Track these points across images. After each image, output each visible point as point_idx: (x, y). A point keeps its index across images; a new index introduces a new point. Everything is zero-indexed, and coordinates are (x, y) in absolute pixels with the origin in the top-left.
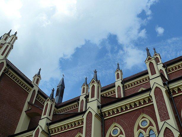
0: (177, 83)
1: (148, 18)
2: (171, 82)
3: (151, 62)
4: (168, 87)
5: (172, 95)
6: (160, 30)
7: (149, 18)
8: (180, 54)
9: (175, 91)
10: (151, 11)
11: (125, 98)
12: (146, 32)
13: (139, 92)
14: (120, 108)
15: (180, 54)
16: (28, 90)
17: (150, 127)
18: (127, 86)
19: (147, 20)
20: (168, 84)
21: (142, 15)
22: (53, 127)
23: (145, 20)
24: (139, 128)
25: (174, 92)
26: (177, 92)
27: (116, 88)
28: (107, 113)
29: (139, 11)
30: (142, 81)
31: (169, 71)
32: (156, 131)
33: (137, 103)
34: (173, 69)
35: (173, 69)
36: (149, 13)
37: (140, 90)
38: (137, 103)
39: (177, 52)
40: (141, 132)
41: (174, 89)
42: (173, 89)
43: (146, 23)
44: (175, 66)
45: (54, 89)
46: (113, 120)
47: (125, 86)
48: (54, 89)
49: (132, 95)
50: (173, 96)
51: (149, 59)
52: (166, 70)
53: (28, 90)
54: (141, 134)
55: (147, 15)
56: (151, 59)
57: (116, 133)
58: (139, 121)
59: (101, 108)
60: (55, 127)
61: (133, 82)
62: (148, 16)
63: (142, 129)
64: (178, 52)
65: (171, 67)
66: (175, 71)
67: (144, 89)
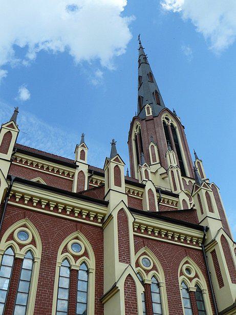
0: (32, 190)
1: (24, 61)
2: (18, 180)
3: (11, 133)
4: (11, 186)
5: (8, 200)
6: (25, 94)
7: (25, 63)
8: (24, 143)
9: (17, 196)
10: (36, 56)
11: (80, 196)
12: (5, 76)
13: (31, 182)
14: (30, 197)
15: (24, 143)
16: (176, 206)
17: (84, 257)
18: (19, 159)
19: (21, 63)
20: (13, 181)
21: (20, 51)
22: (20, 190)
23: (18, 60)
24: (11, 237)
25: (14, 197)
26: (17, 200)
27: (77, 172)
28: (18, 197)
29: (22, 45)
30: (56, 170)
31: (16, 159)
32: (164, 282)
33: (61, 208)
34: (21, 161)
35: (21, 161)
36: (32, 56)
37: (34, 180)
38: (61, 208)
39: (23, 138)
40: (66, 258)
41: (50, 203)
42: (15, 192)
43: (15, 64)
44: (49, 166)
45: (18, 108)
46: (25, 213)
47: (15, 156)
48: (113, 140)
49: (63, 190)
50: (9, 202)
51: (12, 126)
52: (89, 177)
53: (176, 206)
54: (29, 253)
55: (26, 56)
56: (14, 128)
57: (144, 263)
58: (69, 241)
59: (13, 181)
60: (26, 192)
61: (31, 161)
62: (27, 59)
63: (82, 256)
64: (25, 138)
65: (21, 156)
66: (22, 167)
67: (43, 182)
